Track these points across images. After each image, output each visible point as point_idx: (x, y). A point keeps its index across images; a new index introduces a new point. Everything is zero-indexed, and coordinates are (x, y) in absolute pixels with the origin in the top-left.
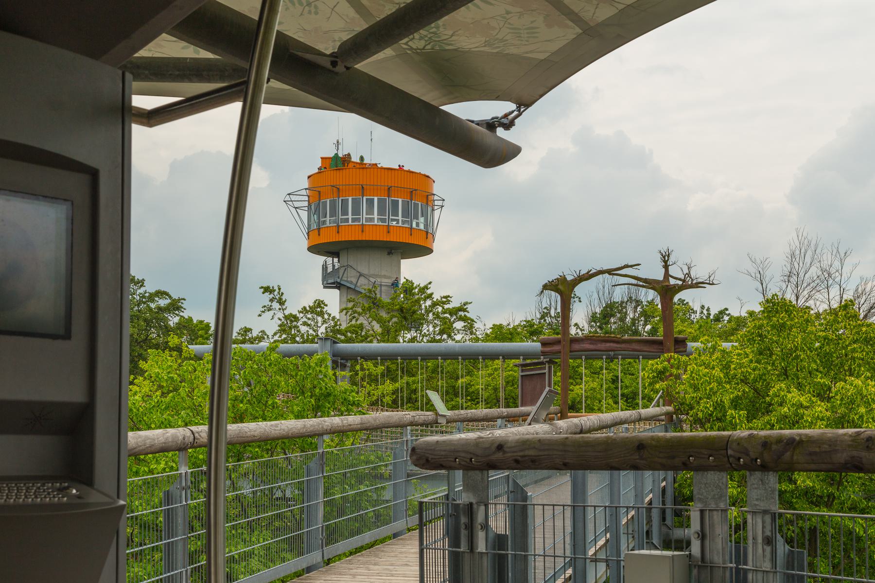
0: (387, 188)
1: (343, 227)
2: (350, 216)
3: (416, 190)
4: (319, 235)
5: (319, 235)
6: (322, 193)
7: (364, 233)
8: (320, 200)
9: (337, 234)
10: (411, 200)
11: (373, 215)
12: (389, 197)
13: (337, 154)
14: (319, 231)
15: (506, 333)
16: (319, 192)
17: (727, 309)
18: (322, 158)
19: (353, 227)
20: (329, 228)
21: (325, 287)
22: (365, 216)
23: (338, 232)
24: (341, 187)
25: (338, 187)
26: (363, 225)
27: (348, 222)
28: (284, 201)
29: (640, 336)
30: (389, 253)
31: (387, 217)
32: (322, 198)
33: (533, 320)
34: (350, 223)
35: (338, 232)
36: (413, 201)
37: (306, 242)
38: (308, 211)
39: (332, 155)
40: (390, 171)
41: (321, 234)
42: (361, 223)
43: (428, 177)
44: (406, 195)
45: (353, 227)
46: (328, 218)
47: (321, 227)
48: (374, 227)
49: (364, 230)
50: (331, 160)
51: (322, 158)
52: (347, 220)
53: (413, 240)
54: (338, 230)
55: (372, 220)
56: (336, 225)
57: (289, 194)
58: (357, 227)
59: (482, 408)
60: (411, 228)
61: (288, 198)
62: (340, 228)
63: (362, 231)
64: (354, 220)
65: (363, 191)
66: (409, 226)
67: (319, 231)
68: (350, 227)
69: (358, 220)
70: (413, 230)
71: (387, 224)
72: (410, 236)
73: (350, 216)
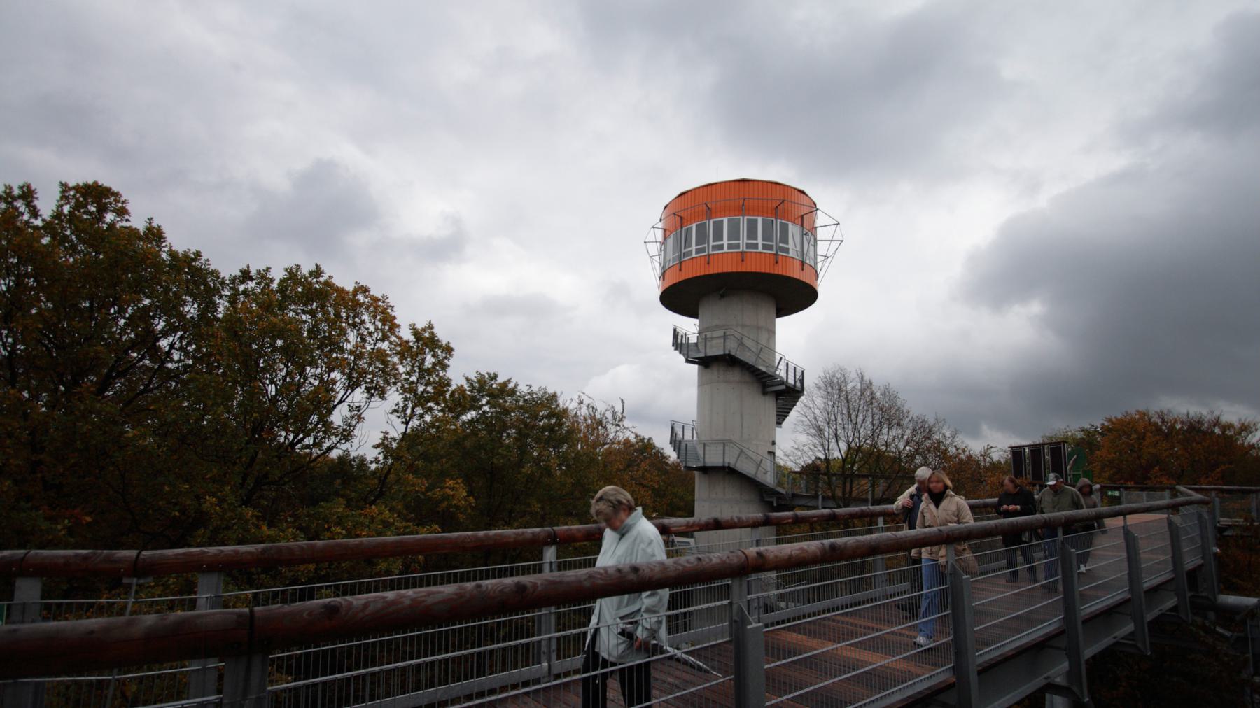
2: (725, 242)
7: (744, 263)
8: (682, 227)
11: (756, 239)
12: (776, 219)
15: (168, 580)
16: (682, 218)
19: (699, 259)
20: (695, 260)
21: (449, 350)
22: (745, 241)
26: (709, 255)
29: (662, 653)
33: (899, 398)
35: (708, 263)
36: (779, 221)
41: (683, 269)
43: (802, 192)
45: (763, 256)
46: (694, 247)
47: (683, 260)
52: (721, 247)
53: (780, 269)
55: (721, 247)
59: (719, 545)
64: (730, 246)
65: (710, 213)
69: (702, 250)
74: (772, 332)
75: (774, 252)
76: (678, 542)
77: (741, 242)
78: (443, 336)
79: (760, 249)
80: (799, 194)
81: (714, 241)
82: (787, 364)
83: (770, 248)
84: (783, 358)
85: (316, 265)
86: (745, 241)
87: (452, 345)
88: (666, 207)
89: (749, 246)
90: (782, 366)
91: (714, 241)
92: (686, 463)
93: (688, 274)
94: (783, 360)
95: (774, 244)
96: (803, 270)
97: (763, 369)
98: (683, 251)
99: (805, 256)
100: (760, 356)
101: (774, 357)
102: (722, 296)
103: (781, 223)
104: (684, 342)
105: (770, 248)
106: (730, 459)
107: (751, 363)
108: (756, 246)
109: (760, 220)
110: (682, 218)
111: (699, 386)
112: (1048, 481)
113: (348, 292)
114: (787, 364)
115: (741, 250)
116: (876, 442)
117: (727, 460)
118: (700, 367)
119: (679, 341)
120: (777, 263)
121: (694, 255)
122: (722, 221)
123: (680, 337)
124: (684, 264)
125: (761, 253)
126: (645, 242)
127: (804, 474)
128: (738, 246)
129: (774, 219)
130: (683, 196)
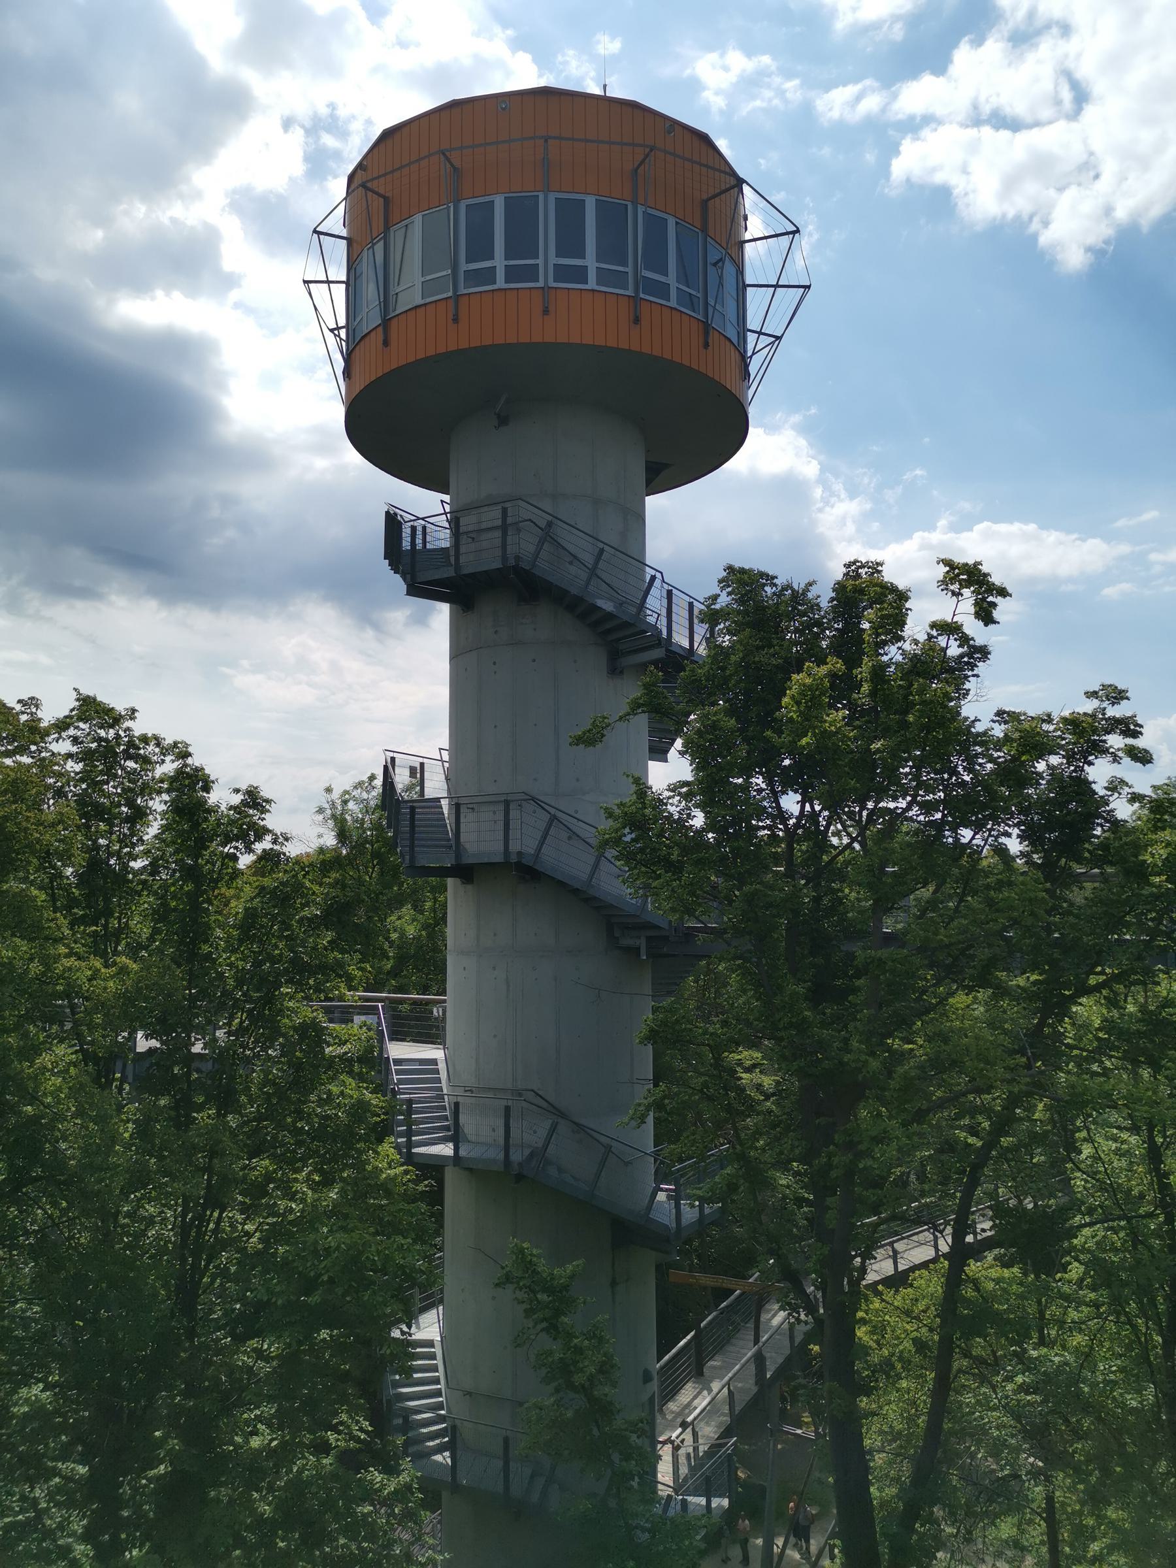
12: (635, 203)
16: (386, 200)
23: (456, 320)
34: (500, 282)
35: (456, 320)
36: (641, 209)
64: (512, 274)
73: (499, 262)
74: (638, 517)
75: (630, 292)
76: (398, 1062)
78: (265, 793)
79: (500, 282)
82: (670, 593)
83: (619, 279)
84: (658, 575)
85: (75, 689)
86: (553, 260)
89: (563, 273)
90: (655, 601)
92: (412, 859)
93: (402, 354)
94: (657, 583)
95: (629, 269)
97: (607, 606)
99: (710, 310)
100: (599, 572)
101: (644, 576)
102: (503, 421)
104: (419, 546)
106: (524, 842)
107: (574, 591)
110: (386, 200)
111: (451, 659)
113: (336, 850)
114: (670, 593)
115: (541, 284)
117: (514, 847)
118: (454, 606)
119: (406, 544)
120: (637, 320)
123: (406, 531)
125: (593, 290)
126: (305, 282)
127: (938, 1003)
128: (530, 273)
129: (629, 204)
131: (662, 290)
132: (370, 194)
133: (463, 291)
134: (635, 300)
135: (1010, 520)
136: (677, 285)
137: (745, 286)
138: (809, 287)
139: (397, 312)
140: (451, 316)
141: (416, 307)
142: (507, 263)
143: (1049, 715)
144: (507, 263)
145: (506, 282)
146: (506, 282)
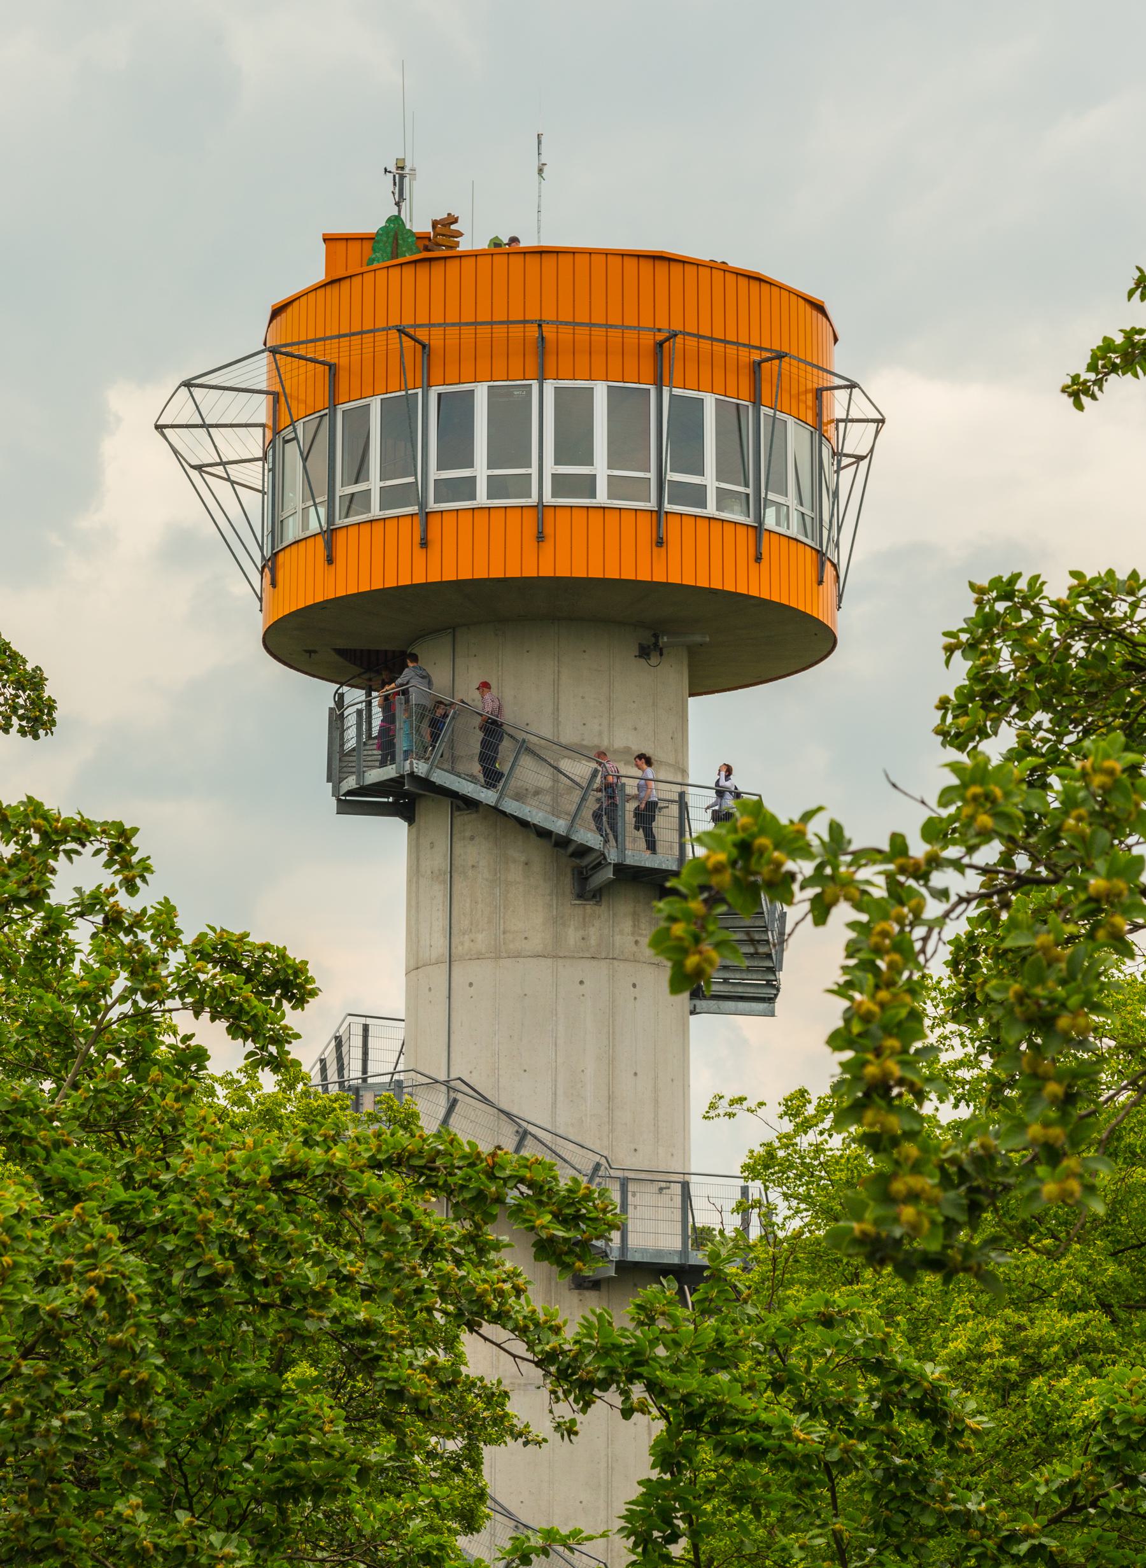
0: (648, 340)
1: (449, 520)
2: (481, 470)
3: (780, 356)
4: (330, 560)
5: (330, 560)
6: (343, 377)
7: (548, 546)
8: (333, 405)
9: (419, 553)
10: (757, 402)
12: (659, 383)
13: (396, 220)
14: (330, 546)
16: (333, 369)
17: (247, 935)
18: (327, 239)
19: (497, 517)
20: (378, 528)
22: (550, 468)
23: (424, 544)
24: (436, 339)
25: (422, 334)
27: (474, 498)
28: (157, 427)
30: (644, 653)
31: (652, 475)
32: (343, 395)
34: (482, 498)
35: (424, 544)
37: (261, 616)
38: (395, 230)
39: (372, 224)
40: (662, 267)
42: (534, 500)
43: (820, 308)
44: (732, 378)
46: (374, 483)
48: (596, 518)
49: (548, 530)
50: (367, 245)
51: (327, 239)
52: (466, 488)
54: (425, 530)
56: (414, 509)
57: (188, 384)
58: (514, 518)
60: (758, 529)
61: (182, 410)
62: (434, 522)
63: (540, 537)
64: (497, 487)
66: (750, 521)
67: (330, 546)
68: (481, 518)
70: (765, 536)
71: (652, 505)
72: (753, 565)
73: (481, 470)
77: (534, 471)
79: (482, 498)
80: (808, 308)
81: (440, 467)
85: (1121, 331)
87: (936, 702)
88: (276, 312)
89: (562, 484)
91: (440, 467)
96: (758, 559)
98: (342, 491)
103: (672, 396)
105: (635, 488)
108: (588, 485)
109: (600, 391)
110: (333, 369)
112: (664, 1277)
116: (941, 1050)
120: (660, 542)
121: (376, 511)
122: (471, 392)
124: (341, 537)
128: (521, 485)
130: (336, 286)
131: (697, 495)
132: (405, 338)
133: (668, 507)
134: (659, 514)
135: (377, 780)
136: (717, 484)
137: (264, 459)
138: (883, 421)
139: (285, 544)
140: (417, 539)
141: (297, 542)
142: (610, 472)
143: (70, 859)
144: (610, 472)
145: (609, 498)
146: (609, 498)
